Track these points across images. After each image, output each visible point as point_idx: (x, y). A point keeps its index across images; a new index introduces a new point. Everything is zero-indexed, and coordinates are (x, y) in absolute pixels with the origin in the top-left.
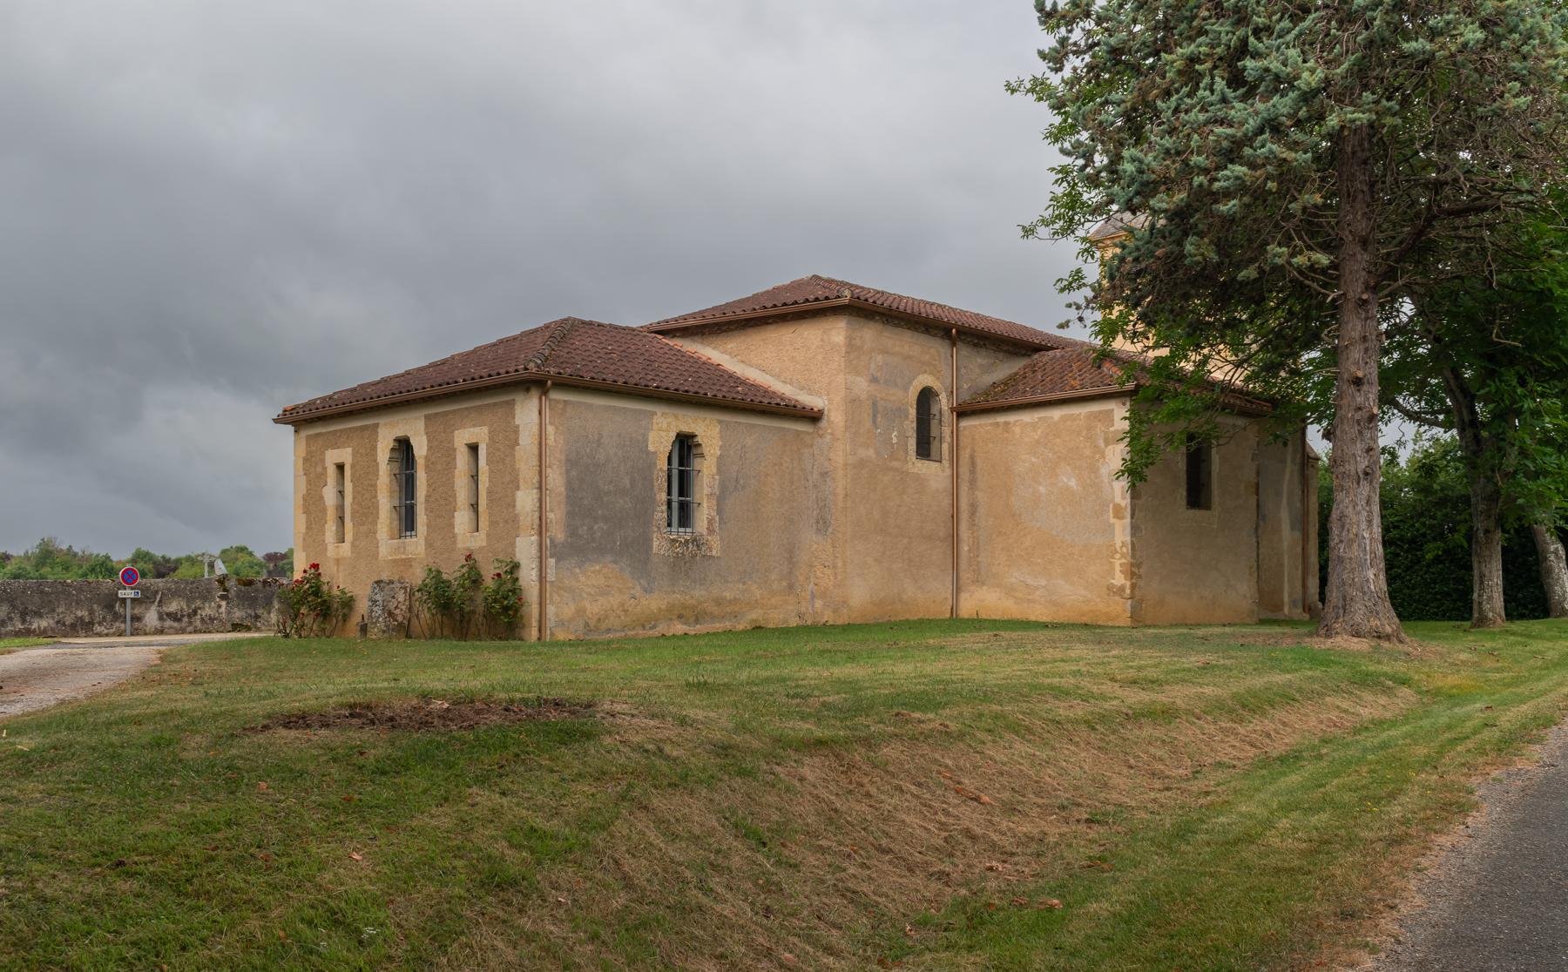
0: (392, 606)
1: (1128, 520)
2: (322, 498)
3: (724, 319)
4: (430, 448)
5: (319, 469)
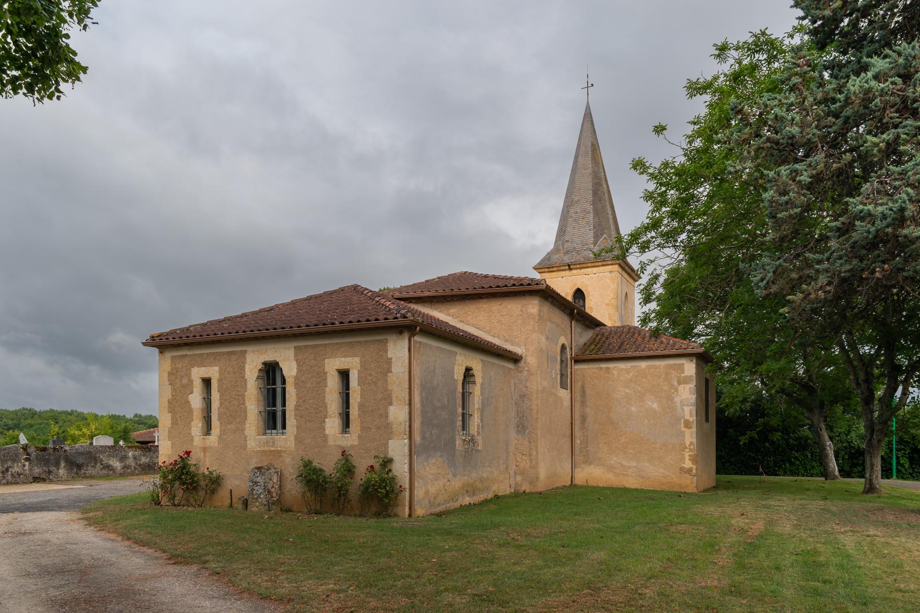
0: (270, 486)
1: (694, 429)
2: (188, 402)
3: (459, 293)
4: (299, 371)
5: (185, 381)
